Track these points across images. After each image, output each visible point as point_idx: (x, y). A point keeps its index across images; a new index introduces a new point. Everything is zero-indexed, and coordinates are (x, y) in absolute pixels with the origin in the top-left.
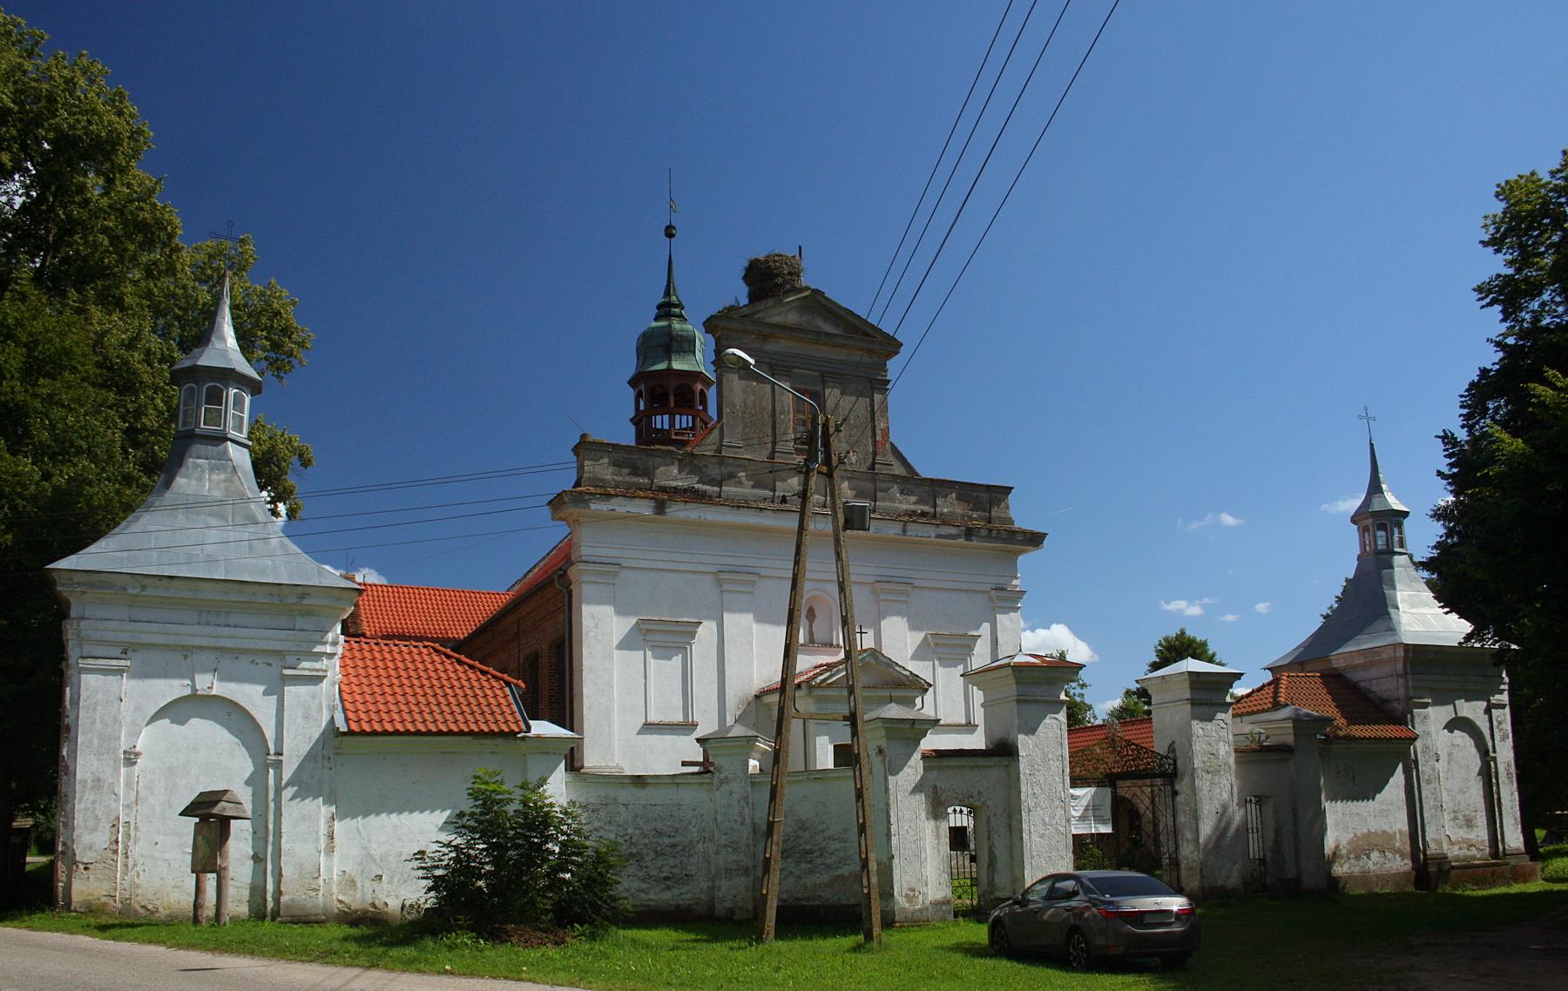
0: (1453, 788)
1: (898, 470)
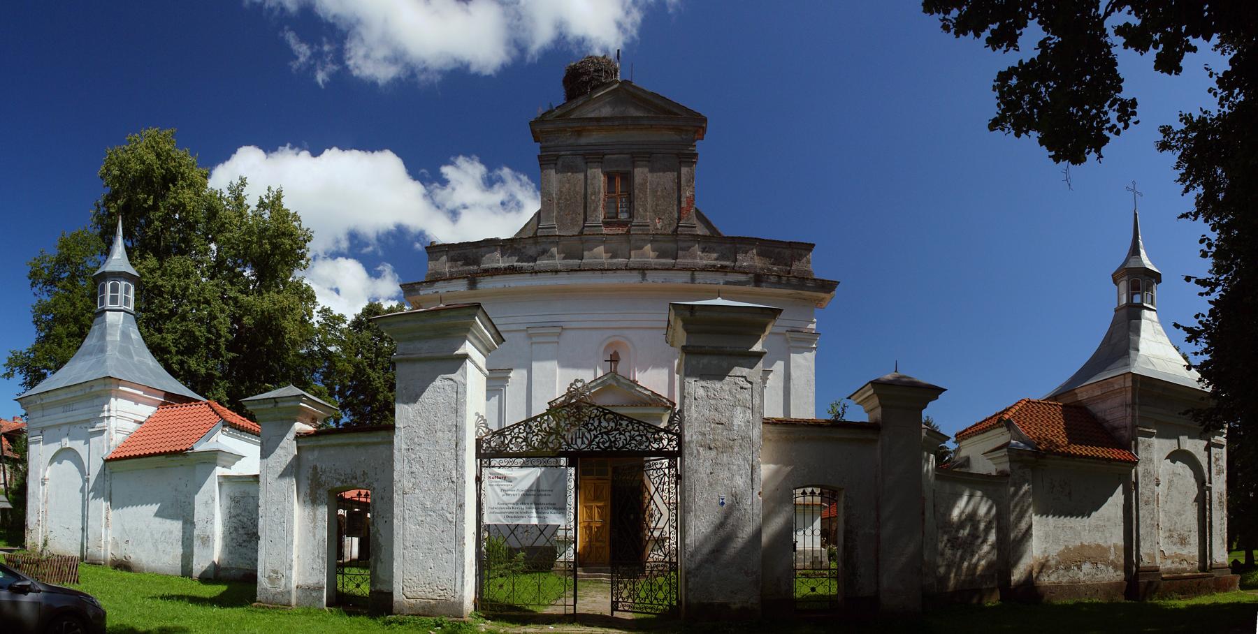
0: (1171, 504)
1: (701, 230)
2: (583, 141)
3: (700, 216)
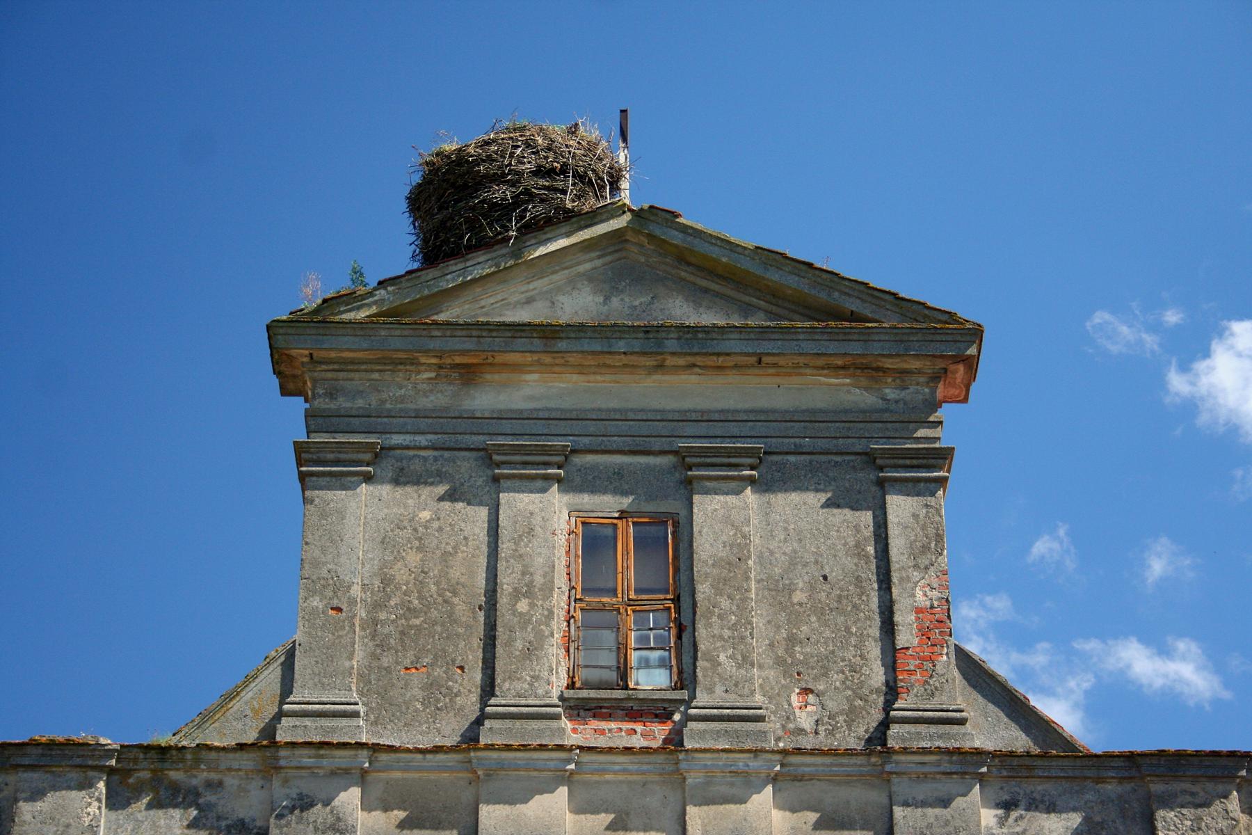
1: (988, 731)
3: (976, 673)
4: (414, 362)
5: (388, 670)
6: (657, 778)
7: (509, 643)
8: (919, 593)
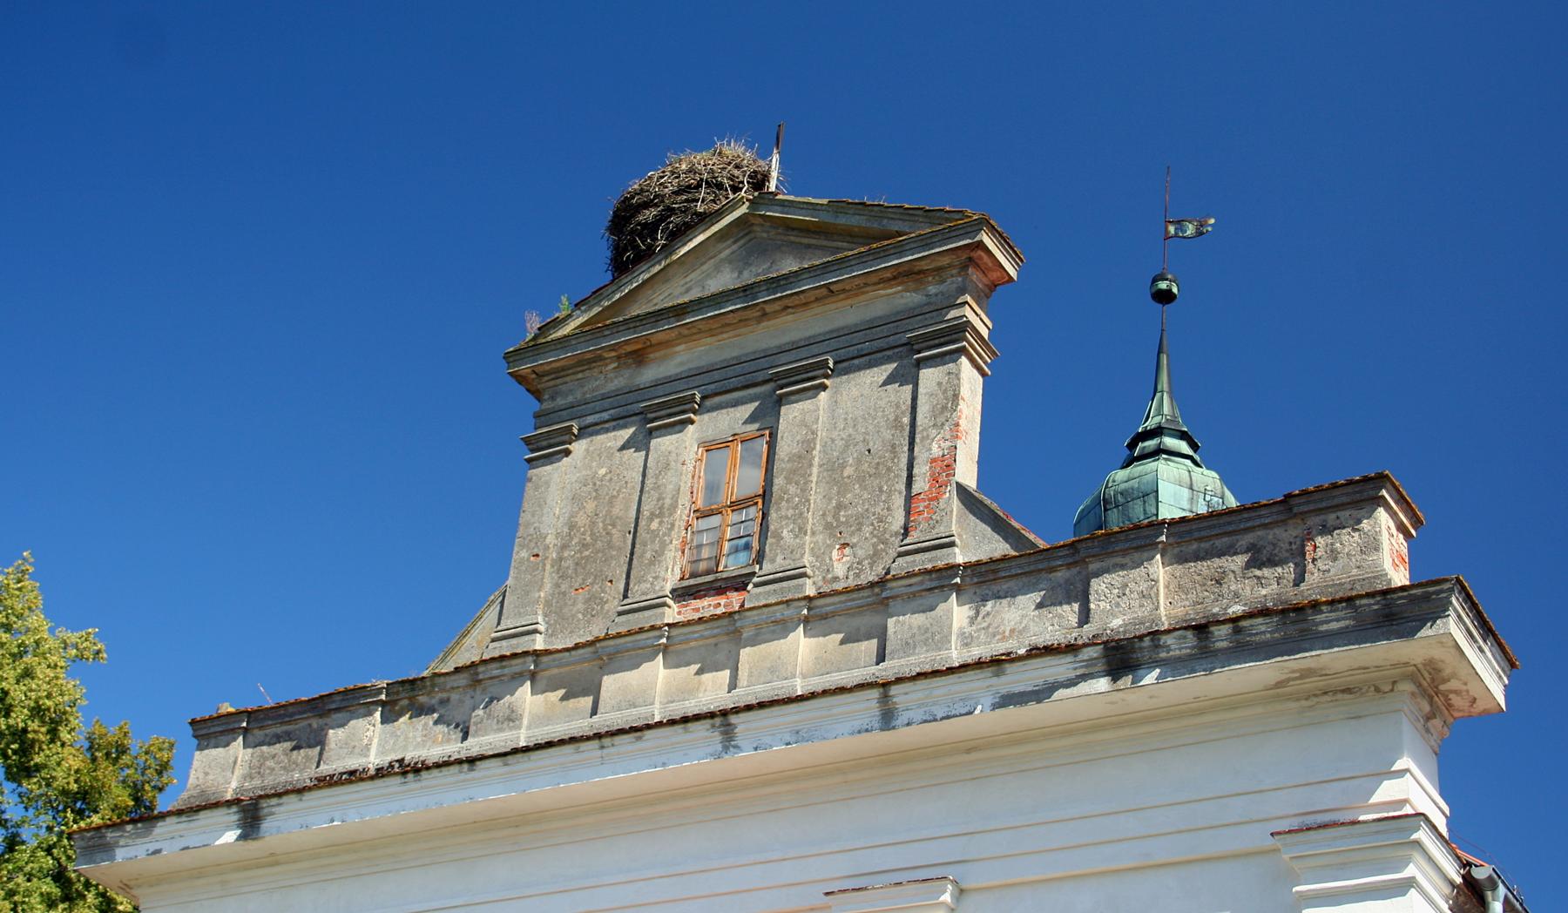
2: (649, 374)
4: (600, 358)
5: (564, 594)
6: (725, 638)
7: (642, 556)
8: (935, 446)
